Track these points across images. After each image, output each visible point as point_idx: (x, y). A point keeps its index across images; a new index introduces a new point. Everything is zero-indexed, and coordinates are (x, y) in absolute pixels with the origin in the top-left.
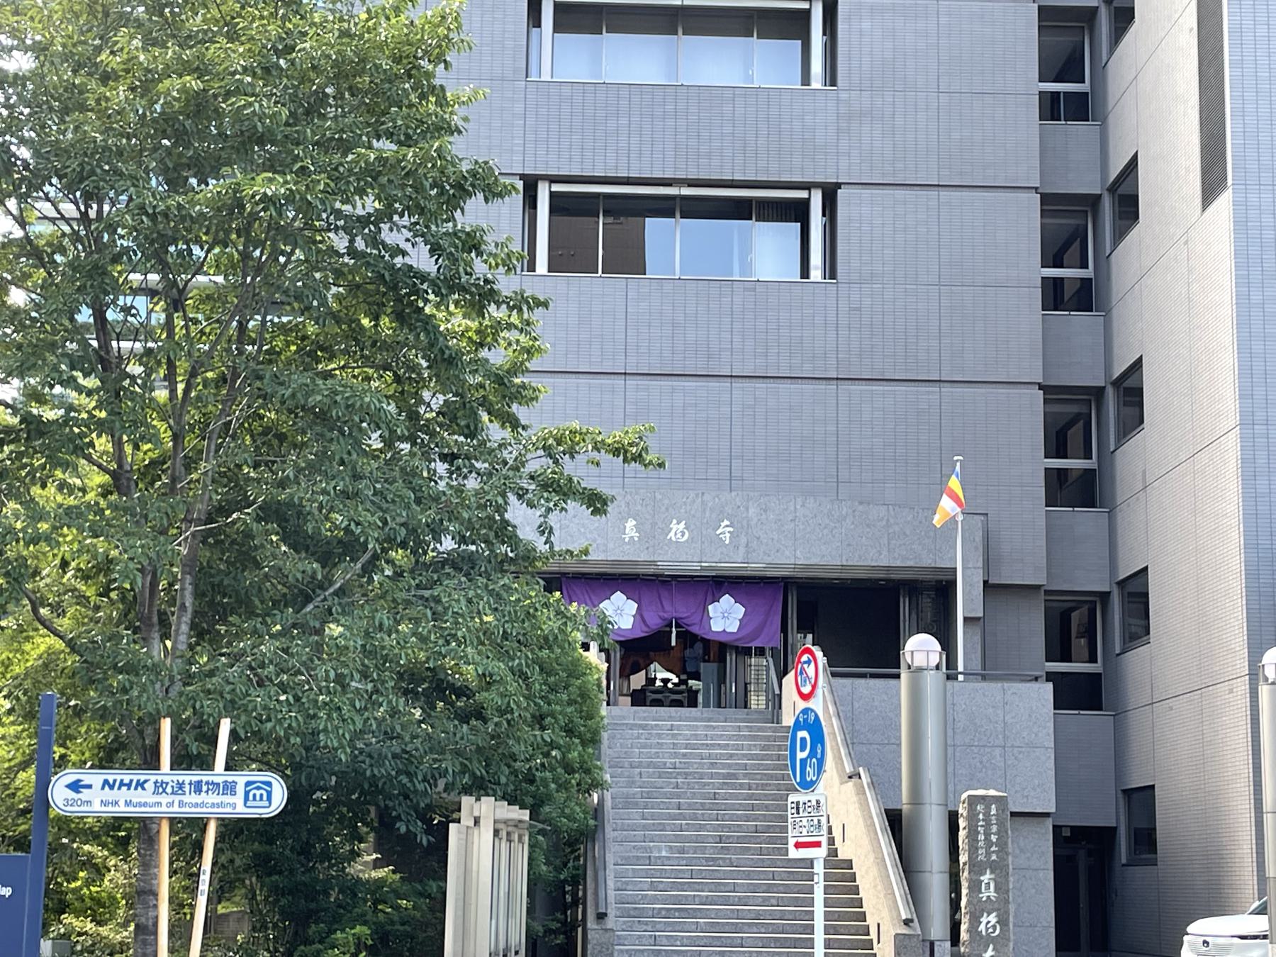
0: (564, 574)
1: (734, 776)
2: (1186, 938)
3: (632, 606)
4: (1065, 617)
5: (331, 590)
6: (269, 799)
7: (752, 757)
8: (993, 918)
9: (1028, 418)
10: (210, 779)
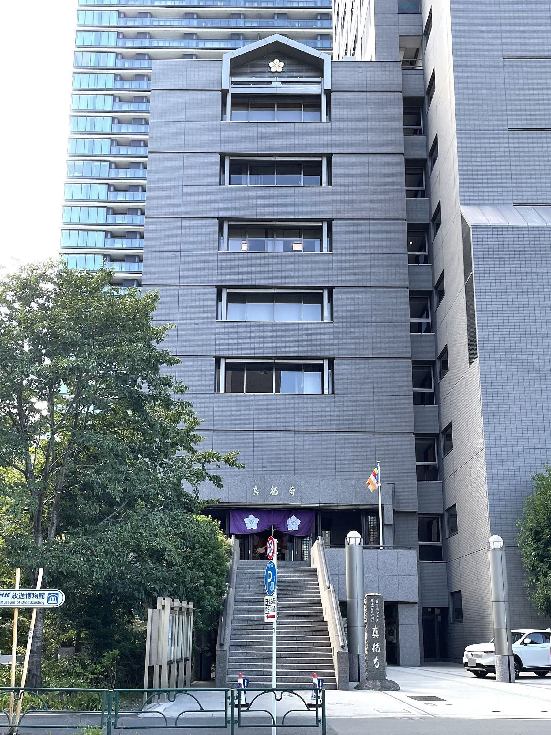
0: (230, 508)
1: (286, 588)
2: (465, 653)
3: (257, 520)
4: (429, 524)
5: (110, 516)
6: (57, 600)
7: (293, 580)
8: (377, 645)
9: (409, 445)
10: (34, 592)
